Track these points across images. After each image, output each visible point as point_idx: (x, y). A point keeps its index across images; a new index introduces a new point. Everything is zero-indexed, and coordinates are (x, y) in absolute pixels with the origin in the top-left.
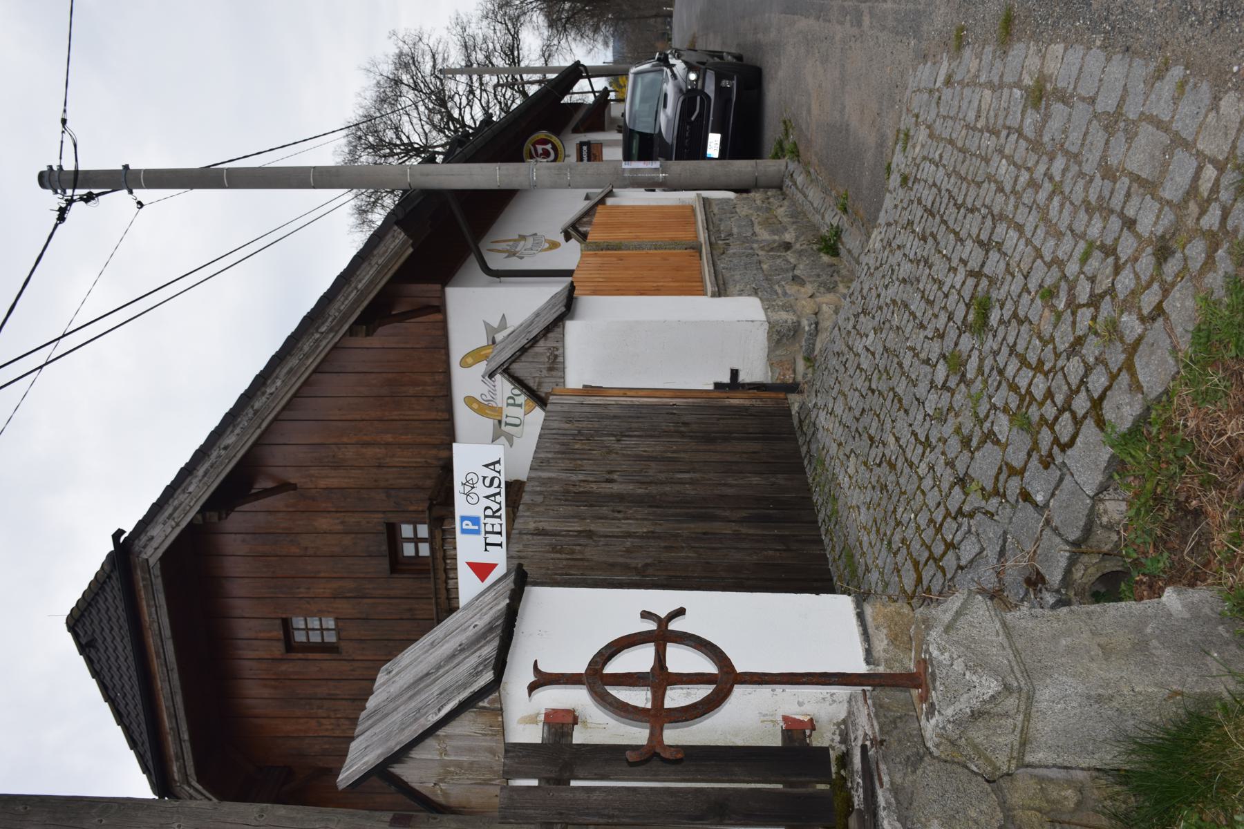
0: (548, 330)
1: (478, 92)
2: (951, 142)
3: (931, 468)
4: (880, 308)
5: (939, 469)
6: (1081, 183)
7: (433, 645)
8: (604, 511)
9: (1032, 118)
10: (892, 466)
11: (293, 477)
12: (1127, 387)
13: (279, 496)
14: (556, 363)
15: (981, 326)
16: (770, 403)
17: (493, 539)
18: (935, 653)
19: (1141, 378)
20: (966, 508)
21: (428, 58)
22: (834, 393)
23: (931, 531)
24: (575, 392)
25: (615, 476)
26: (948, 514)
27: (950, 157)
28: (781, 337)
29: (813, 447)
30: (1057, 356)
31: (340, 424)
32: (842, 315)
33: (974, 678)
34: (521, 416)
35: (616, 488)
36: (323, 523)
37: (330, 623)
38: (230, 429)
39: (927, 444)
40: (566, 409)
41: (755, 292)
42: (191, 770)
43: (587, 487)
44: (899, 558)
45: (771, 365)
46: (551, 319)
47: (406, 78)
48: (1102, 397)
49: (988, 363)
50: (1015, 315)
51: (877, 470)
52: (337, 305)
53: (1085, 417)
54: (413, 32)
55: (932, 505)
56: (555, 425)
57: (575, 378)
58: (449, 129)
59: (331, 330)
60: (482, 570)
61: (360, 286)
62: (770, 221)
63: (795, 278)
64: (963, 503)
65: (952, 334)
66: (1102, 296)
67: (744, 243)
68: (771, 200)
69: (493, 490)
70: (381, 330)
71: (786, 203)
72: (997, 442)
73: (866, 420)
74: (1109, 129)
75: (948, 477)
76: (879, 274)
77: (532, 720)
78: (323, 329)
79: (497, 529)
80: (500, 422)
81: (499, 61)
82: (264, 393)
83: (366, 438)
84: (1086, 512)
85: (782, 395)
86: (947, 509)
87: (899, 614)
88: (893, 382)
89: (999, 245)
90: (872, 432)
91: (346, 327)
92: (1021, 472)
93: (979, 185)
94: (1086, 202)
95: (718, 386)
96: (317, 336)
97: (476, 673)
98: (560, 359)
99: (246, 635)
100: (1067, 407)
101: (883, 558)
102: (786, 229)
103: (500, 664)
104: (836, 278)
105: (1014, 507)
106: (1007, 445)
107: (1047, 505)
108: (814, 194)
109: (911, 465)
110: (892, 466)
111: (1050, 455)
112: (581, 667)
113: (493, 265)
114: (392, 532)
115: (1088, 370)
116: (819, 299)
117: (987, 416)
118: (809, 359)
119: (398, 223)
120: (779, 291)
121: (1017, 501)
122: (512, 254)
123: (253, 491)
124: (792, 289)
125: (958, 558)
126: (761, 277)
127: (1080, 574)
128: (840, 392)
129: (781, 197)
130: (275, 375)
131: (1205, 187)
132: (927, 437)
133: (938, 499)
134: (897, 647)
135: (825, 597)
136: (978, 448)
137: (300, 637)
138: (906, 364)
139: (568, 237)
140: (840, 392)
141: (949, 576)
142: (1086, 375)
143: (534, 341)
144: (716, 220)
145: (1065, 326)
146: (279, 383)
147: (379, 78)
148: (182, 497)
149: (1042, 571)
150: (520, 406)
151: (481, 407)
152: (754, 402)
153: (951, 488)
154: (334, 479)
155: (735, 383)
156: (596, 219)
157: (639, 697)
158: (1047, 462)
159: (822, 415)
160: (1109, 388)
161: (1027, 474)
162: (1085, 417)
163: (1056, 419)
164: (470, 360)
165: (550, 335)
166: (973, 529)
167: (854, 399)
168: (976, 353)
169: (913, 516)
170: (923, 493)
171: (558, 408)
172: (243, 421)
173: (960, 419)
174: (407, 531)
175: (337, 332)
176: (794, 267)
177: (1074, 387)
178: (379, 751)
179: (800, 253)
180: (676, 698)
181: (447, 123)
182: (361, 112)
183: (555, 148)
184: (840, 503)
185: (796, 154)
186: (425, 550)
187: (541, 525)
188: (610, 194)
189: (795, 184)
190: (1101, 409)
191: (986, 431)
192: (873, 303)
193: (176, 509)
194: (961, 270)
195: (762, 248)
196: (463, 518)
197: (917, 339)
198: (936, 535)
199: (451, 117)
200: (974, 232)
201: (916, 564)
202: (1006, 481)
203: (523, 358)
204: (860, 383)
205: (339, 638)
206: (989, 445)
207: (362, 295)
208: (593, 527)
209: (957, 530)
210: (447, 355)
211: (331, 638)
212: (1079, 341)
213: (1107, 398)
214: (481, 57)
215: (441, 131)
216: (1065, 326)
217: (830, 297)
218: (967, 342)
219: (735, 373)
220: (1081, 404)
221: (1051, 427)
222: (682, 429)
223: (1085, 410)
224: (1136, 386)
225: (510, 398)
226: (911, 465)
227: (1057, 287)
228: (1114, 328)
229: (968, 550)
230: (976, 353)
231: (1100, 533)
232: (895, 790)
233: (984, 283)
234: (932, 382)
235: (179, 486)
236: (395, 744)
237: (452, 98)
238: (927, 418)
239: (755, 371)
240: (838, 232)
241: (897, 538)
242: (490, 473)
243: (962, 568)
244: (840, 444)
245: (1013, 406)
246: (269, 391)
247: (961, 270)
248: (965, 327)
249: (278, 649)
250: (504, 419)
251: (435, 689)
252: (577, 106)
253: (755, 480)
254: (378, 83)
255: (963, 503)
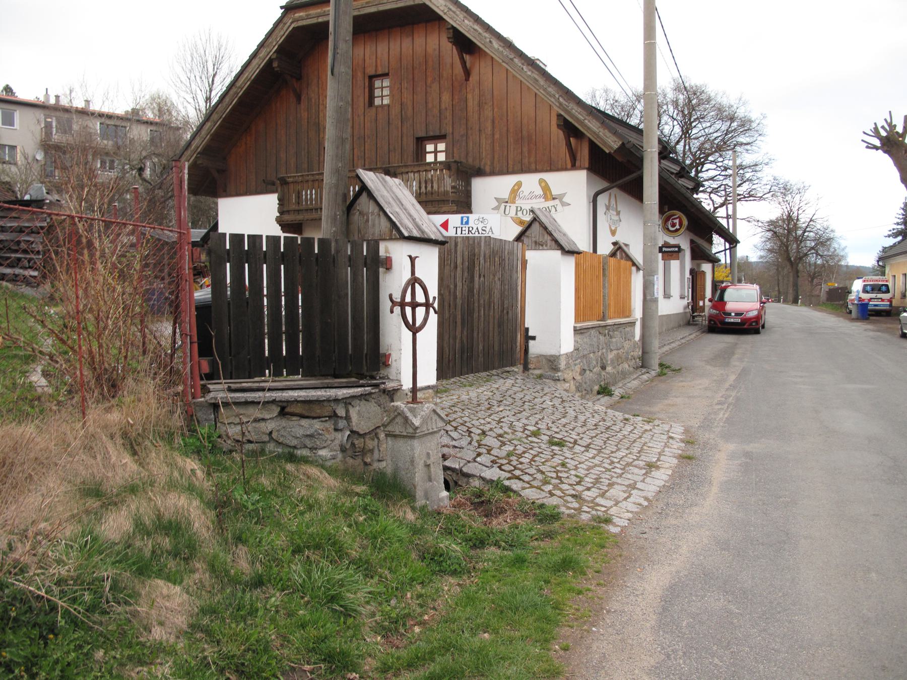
0: (556, 241)
1: (723, 173)
2: (640, 437)
4: (564, 407)
5: (488, 425)
6: (609, 477)
7: (413, 205)
8: (466, 274)
9: (642, 464)
10: (489, 409)
11: (474, 78)
13: (461, 70)
14: (538, 245)
15: (551, 443)
16: (518, 356)
17: (459, 230)
18: (426, 406)
20: (472, 435)
21: (747, 140)
22: (523, 387)
24: (523, 256)
25: (482, 279)
27: (633, 437)
28: (552, 362)
29: (496, 377)
30: (537, 466)
31: (505, 107)
32: (562, 392)
34: (510, 215)
35: (476, 279)
36: (446, 97)
37: (386, 101)
38: (502, 45)
40: (515, 252)
41: (576, 349)
42: (300, 23)
43: (477, 265)
44: (448, 410)
45: (538, 357)
46: (562, 243)
47: (735, 124)
49: (535, 445)
50: (555, 454)
51: (486, 403)
52: (575, 108)
54: (765, 130)
55: (473, 422)
56: (507, 247)
57: (533, 257)
58: (700, 154)
59: (561, 104)
60: (445, 225)
61: (586, 121)
62: (620, 360)
63: (584, 370)
65: (549, 433)
66: (561, 480)
67: (606, 344)
68: (634, 361)
69: (480, 231)
70: (561, 133)
71: (631, 369)
72: (501, 446)
73: (510, 399)
74: (629, 486)
75: (486, 428)
76: (581, 407)
77: (387, 251)
78: (561, 99)
79: (463, 232)
80: (507, 202)
81: (745, 187)
82: (523, 64)
83: (496, 122)
85: (522, 362)
88: (527, 410)
89: (587, 451)
90: (504, 402)
91: (563, 113)
93: (616, 446)
94: (601, 478)
95: (527, 329)
96: (557, 96)
97: (406, 228)
98: (541, 248)
99: (379, 49)
100: (515, 468)
101: (447, 404)
102: (614, 368)
103: (411, 239)
104: (584, 392)
105: (474, 451)
108: (635, 383)
109: (490, 416)
110: (489, 409)
111: (496, 463)
112: (417, 275)
113: (599, 198)
114: (440, 137)
115: (531, 475)
116: (572, 382)
118: (540, 377)
119: (623, 144)
120: (577, 362)
122: (608, 208)
123: (464, 55)
124: (578, 369)
126: (586, 352)
128: (523, 390)
129: (635, 366)
130: (534, 71)
131: (598, 508)
135: (435, 373)
137: (378, 83)
138: (536, 416)
139: (615, 244)
140: (523, 390)
142: (529, 474)
143: (550, 234)
144: (621, 329)
145: (549, 469)
146: (529, 73)
147: (735, 107)
148: (461, 16)
150: (516, 214)
151: (515, 191)
152: (518, 347)
154: (472, 103)
155: (528, 338)
156: (623, 262)
157: (408, 299)
158: (493, 462)
159: (512, 382)
160: (524, 481)
164: (543, 184)
165: (553, 242)
167: (520, 395)
168: (540, 441)
171: (515, 248)
172: (506, 52)
174: (442, 146)
175: (559, 107)
176: (591, 371)
178: (373, 187)
179: (600, 375)
180: (408, 310)
181: (704, 153)
182: (713, 95)
183: (677, 230)
184: (469, 388)
185: (660, 375)
186: (430, 158)
187: (459, 244)
188: (638, 269)
189: (642, 374)
192: (567, 405)
193: (454, 12)
194: (578, 437)
195: (603, 354)
196: (468, 218)
197: (546, 420)
199: (709, 155)
200: (594, 443)
203: (541, 228)
204: (527, 398)
205: (377, 107)
206: (500, 443)
207: (581, 123)
208: (458, 269)
210: (547, 171)
211: (377, 102)
212: (543, 473)
214: (748, 175)
215: (700, 149)
216: (549, 469)
217: (573, 388)
218: (545, 438)
219: (534, 338)
220: (517, 473)
222: (505, 312)
224: (524, 488)
225: (521, 208)
226: (490, 416)
227: (566, 467)
228: (546, 482)
229: (455, 435)
230: (540, 441)
231: (465, 480)
232: (370, 394)
233: (571, 445)
234: (527, 425)
235: (468, 14)
236: (376, 194)
237: (721, 156)
239: (535, 348)
240: (610, 394)
241: (456, 409)
242: (488, 229)
244: (498, 388)
245: (517, 452)
246: (525, 67)
247: (578, 437)
248: (551, 437)
249: (371, 71)
250: (508, 205)
251: (398, 210)
252: (710, 242)
253: (481, 347)
254: (732, 106)
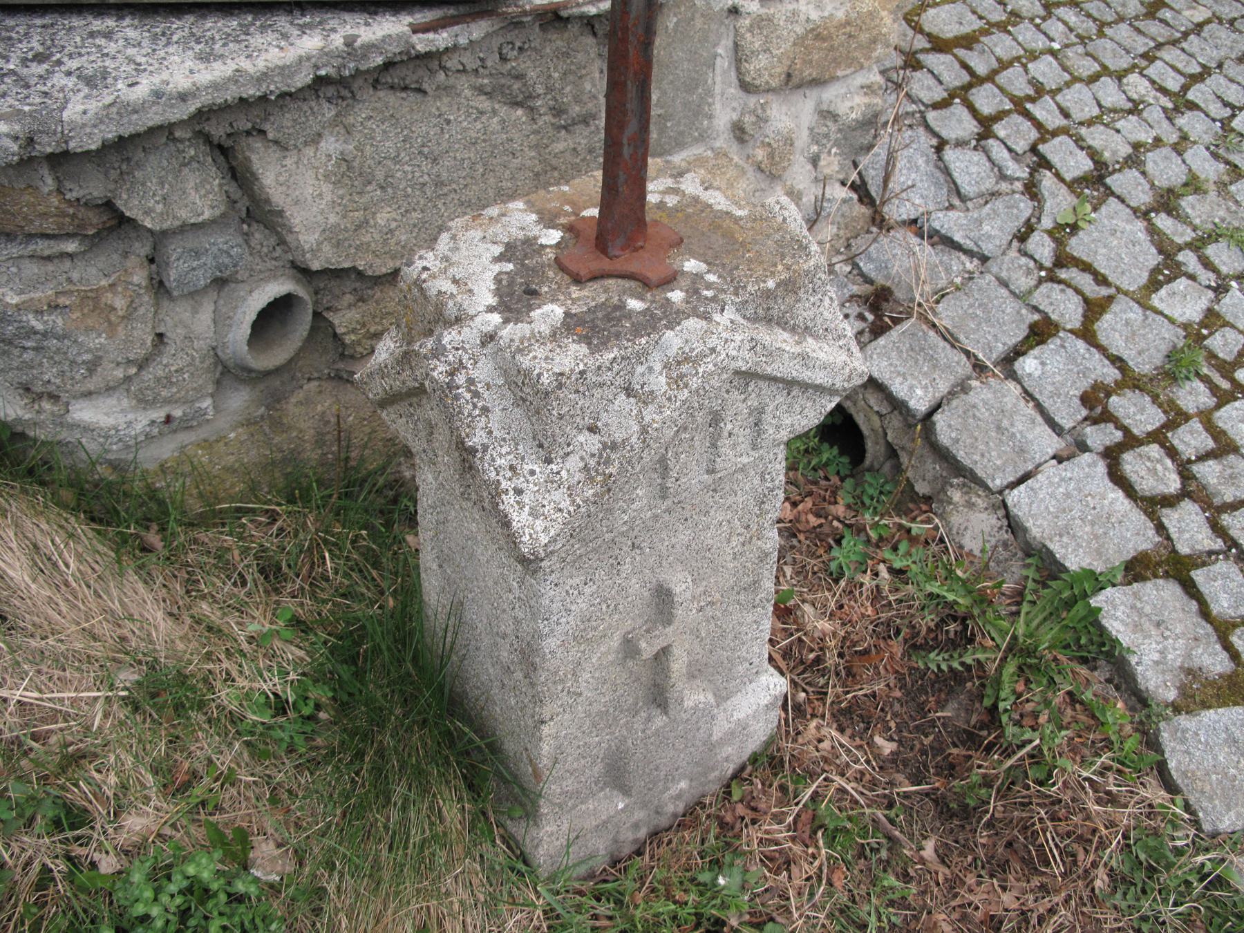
3: (1136, 108)
5: (1129, 125)
12: (1196, 663)
19: (1209, 716)
20: (1047, 180)
23: (1021, 88)
26: (1046, 134)
33: (574, 463)
39: (1181, 104)
48: (1190, 589)
53: (1160, 528)
55: (1067, 98)
64: (1058, 175)
72: (1154, 284)
84: (980, 473)
86: (1055, 133)
87: (874, 41)
92: (1087, 334)
106: (1146, 306)
107: (1012, 375)
109: (1149, 57)
111: (1106, 417)
117: (1207, 264)
121: (1035, 309)
125: (960, 144)
127: (872, 402)
132: (1193, 106)
133: (1077, 115)
134: (800, 41)
136: (1152, 231)
141: (931, 116)
149: (895, 333)
153: (1093, 154)
161: (1081, 345)
162: (1160, 528)
163: (1172, 453)
166: (1004, 186)
169: (1056, 46)
170: (1094, 78)
173: (1212, 194)
177: (1226, 519)
190: (1167, 575)
191: (1180, 257)
198: (1013, 99)
201: (968, 41)
202: (1078, 291)
209: (1010, 150)
213: (1186, 598)
221: (1157, 437)
223: (1172, 531)
226: (1149, 57)
238: (1227, 112)
243: (939, 149)
255: (1058, 175)
